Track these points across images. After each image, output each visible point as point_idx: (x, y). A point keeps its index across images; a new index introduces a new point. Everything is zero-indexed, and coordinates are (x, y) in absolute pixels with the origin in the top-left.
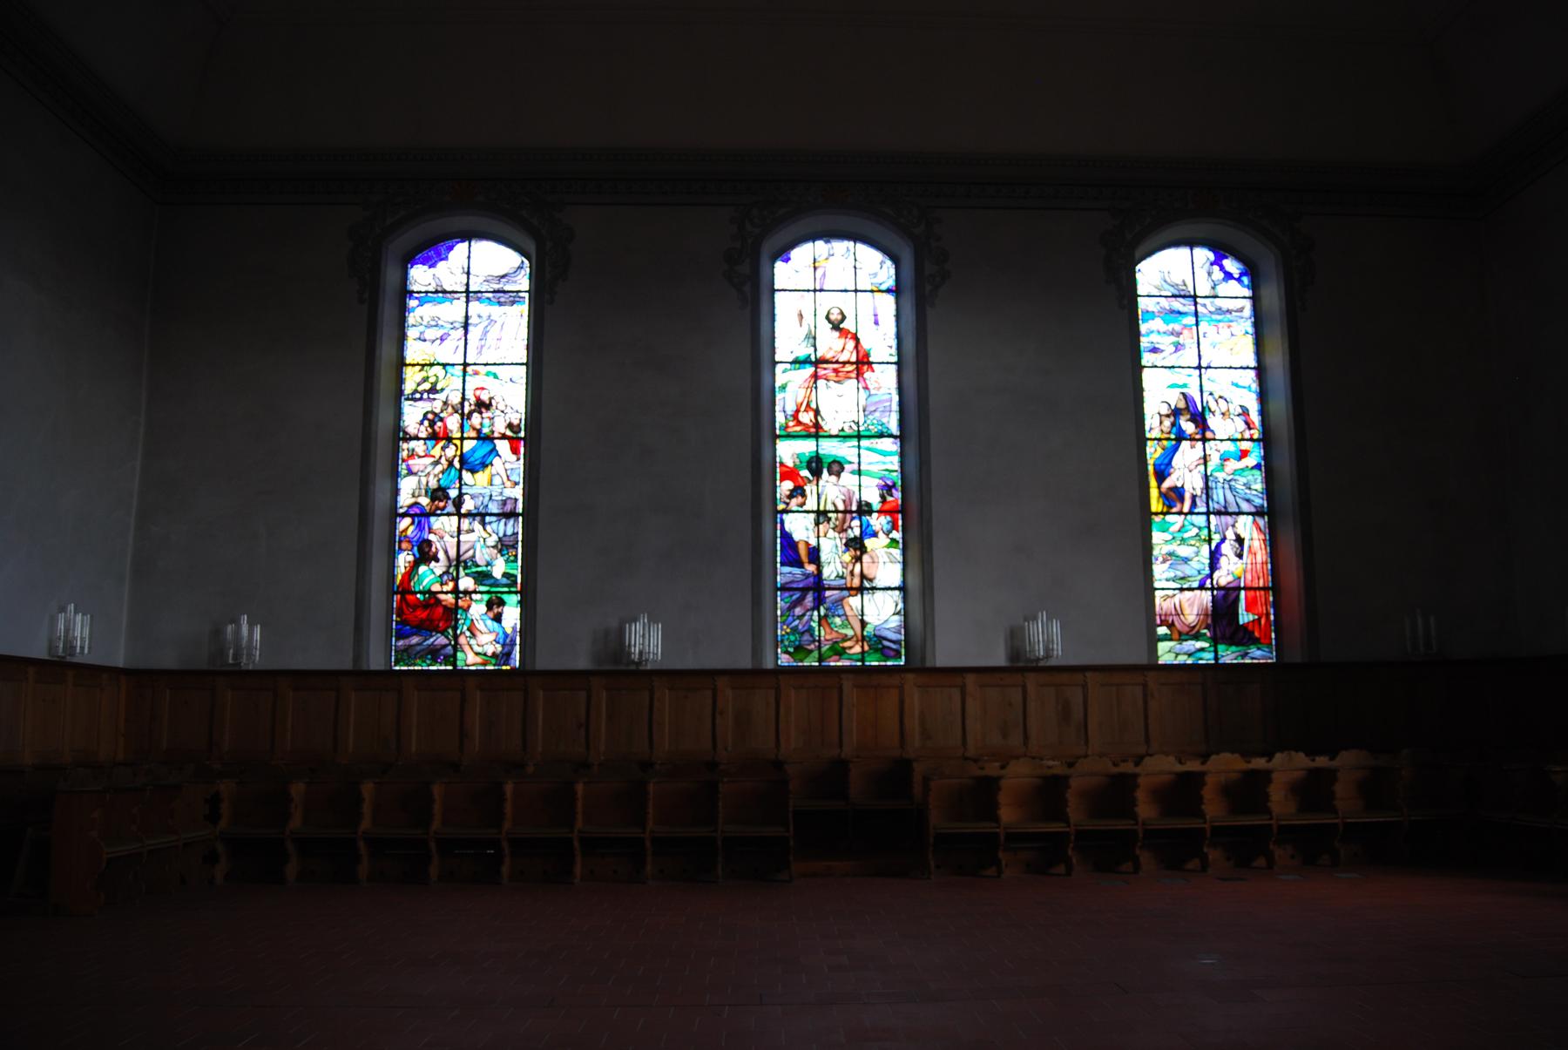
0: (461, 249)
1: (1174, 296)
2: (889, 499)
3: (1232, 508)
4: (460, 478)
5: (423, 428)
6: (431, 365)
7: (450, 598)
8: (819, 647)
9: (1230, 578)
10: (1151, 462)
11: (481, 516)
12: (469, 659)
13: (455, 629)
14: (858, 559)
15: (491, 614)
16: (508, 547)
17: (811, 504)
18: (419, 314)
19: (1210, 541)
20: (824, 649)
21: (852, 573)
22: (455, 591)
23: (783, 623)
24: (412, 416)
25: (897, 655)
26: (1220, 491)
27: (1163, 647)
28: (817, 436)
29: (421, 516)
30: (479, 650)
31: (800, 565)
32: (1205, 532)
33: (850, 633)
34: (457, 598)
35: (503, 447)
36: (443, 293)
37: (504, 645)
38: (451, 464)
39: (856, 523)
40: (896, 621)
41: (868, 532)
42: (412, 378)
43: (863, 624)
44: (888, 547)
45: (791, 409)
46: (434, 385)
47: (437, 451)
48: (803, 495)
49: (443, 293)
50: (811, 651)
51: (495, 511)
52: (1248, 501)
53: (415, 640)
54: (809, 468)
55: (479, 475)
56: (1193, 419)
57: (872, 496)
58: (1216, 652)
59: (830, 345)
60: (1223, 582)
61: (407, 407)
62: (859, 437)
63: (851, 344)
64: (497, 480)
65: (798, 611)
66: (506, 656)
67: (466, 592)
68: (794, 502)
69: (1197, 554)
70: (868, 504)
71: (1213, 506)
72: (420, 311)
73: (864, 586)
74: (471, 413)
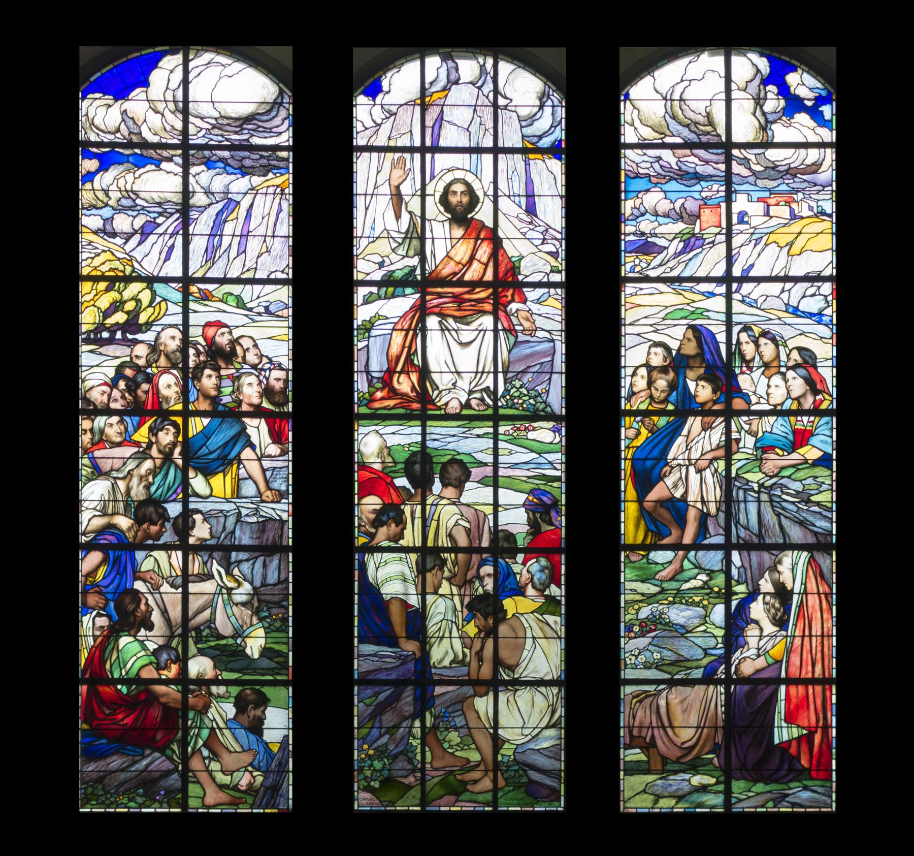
0: (171, 62)
1: (688, 145)
2: (546, 528)
4: (185, 483)
5: (116, 394)
6: (128, 280)
7: (172, 692)
8: (423, 781)
9: (761, 663)
10: (626, 454)
11: (222, 550)
12: (206, 797)
13: (184, 744)
14: (491, 632)
18: (101, 185)
19: (727, 595)
20: (429, 785)
21: (479, 656)
22: (183, 679)
24: (96, 370)
25: (554, 794)
26: (753, 508)
27: (630, 785)
28: (423, 418)
29: (119, 550)
31: (392, 641)
32: (720, 580)
33: (475, 757)
34: (185, 692)
35: (257, 430)
36: (138, 152)
37: (266, 773)
38: (167, 457)
39: (488, 569)
40: (550, 739)
41: (508, 585)
43: (497, 742)
44: (541, 611)
45: (377, 364)
46: (134, 315)
47: (142, 435)
48: (400, 521)
50: (409, 787)
51: (246, 541)
52: (802, 523)
53: (115, 762)
54: (408, 473)
55: (217, 480)
56: (709, 377)
57: (515, 520)
58: (728, 793)
59: (445, 246)
60: (748, 669)
62: (496, 419)
63: (484, 251)
64: (249, 489)
65: (388, 719)
66: (273, 790)
67: (201, 682)
68: (383, 531)
69: (705, 619)
70: (510, 537)
72: (105, 179)
73: (500, 679)
74: (200, 368)
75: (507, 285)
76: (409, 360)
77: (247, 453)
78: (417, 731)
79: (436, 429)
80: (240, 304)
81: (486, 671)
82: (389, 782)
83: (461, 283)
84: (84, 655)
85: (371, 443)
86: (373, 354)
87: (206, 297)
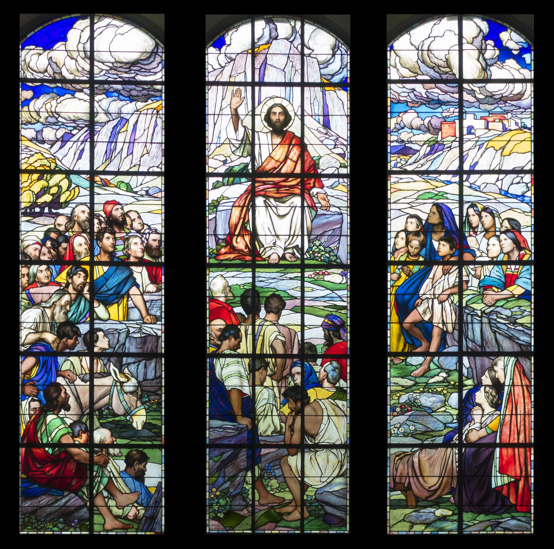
0: (82, 24)
2: (336, 341)
3: (492, 348)
4: (92, 311)
5: (45, 250)
7: (83, 452)
8: (253, 513)
9: (483, 433)
11: (116, 356)
12: (106, 524)
14: (299, 412)
15: (132, 471)
16: (149, 393)
17: (245, 347)
18: (35, 109)
19: (460, 386)
20: (257, 515)
22: (90, 444)
23: (213, 485)
25: (342, 522)
26: (477, 327)
28: (253, 266)
29: (47, 356)
30: (116, 511)
31: (232, 418)
33: (288, 496)
34: (91, 453)
35: (141, 274)
36: (60, 86)
37: (146, 508)
38: (79, 293)
39: (297, 369)
40: (340, 484)
42: (29, 190)
43: (304, 487)
44: (333, 397)
45: (222, 230)
46: (57, 196)
47: (62, 278)
48: (237, 336)
49: (60, 86)
50: (244, 517)
51: (133, 350)
52: (511, 338)
53: (44, 500)
55: (113, 309)
57: (316, 336)
58: (460, 521)
60: (474, 437)
61: (25, 225)
62: (303, 267)
63: (295, 153)
64: (135, 314)
65: (230, 471)
66: (151, 519)
67: (103, 446)
68: (226, 344)
70: (312, 347)
71: (467, 345)
72: (37, 104)
73: (306, 444)
74: (102, 232)
75: (310, 176)
76: (244, 227)
77: (134, 290)
78: (249, 479)
79: (262, 273)
80: (129, 189)
81: (296, 439)
82: (230, 514)
83: (279, 175)
84: (23, 428)
85: (218, 283)
86: (219, 223)
87: (106, 184)
